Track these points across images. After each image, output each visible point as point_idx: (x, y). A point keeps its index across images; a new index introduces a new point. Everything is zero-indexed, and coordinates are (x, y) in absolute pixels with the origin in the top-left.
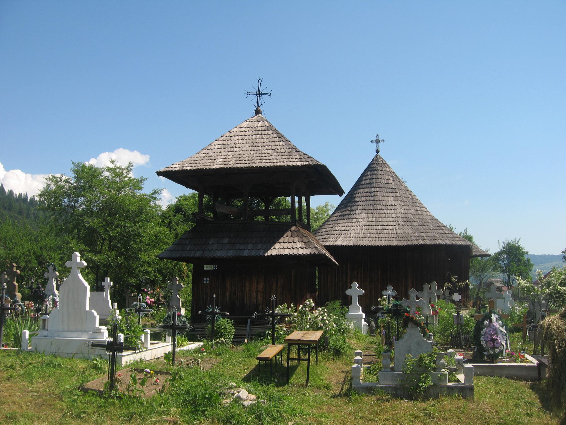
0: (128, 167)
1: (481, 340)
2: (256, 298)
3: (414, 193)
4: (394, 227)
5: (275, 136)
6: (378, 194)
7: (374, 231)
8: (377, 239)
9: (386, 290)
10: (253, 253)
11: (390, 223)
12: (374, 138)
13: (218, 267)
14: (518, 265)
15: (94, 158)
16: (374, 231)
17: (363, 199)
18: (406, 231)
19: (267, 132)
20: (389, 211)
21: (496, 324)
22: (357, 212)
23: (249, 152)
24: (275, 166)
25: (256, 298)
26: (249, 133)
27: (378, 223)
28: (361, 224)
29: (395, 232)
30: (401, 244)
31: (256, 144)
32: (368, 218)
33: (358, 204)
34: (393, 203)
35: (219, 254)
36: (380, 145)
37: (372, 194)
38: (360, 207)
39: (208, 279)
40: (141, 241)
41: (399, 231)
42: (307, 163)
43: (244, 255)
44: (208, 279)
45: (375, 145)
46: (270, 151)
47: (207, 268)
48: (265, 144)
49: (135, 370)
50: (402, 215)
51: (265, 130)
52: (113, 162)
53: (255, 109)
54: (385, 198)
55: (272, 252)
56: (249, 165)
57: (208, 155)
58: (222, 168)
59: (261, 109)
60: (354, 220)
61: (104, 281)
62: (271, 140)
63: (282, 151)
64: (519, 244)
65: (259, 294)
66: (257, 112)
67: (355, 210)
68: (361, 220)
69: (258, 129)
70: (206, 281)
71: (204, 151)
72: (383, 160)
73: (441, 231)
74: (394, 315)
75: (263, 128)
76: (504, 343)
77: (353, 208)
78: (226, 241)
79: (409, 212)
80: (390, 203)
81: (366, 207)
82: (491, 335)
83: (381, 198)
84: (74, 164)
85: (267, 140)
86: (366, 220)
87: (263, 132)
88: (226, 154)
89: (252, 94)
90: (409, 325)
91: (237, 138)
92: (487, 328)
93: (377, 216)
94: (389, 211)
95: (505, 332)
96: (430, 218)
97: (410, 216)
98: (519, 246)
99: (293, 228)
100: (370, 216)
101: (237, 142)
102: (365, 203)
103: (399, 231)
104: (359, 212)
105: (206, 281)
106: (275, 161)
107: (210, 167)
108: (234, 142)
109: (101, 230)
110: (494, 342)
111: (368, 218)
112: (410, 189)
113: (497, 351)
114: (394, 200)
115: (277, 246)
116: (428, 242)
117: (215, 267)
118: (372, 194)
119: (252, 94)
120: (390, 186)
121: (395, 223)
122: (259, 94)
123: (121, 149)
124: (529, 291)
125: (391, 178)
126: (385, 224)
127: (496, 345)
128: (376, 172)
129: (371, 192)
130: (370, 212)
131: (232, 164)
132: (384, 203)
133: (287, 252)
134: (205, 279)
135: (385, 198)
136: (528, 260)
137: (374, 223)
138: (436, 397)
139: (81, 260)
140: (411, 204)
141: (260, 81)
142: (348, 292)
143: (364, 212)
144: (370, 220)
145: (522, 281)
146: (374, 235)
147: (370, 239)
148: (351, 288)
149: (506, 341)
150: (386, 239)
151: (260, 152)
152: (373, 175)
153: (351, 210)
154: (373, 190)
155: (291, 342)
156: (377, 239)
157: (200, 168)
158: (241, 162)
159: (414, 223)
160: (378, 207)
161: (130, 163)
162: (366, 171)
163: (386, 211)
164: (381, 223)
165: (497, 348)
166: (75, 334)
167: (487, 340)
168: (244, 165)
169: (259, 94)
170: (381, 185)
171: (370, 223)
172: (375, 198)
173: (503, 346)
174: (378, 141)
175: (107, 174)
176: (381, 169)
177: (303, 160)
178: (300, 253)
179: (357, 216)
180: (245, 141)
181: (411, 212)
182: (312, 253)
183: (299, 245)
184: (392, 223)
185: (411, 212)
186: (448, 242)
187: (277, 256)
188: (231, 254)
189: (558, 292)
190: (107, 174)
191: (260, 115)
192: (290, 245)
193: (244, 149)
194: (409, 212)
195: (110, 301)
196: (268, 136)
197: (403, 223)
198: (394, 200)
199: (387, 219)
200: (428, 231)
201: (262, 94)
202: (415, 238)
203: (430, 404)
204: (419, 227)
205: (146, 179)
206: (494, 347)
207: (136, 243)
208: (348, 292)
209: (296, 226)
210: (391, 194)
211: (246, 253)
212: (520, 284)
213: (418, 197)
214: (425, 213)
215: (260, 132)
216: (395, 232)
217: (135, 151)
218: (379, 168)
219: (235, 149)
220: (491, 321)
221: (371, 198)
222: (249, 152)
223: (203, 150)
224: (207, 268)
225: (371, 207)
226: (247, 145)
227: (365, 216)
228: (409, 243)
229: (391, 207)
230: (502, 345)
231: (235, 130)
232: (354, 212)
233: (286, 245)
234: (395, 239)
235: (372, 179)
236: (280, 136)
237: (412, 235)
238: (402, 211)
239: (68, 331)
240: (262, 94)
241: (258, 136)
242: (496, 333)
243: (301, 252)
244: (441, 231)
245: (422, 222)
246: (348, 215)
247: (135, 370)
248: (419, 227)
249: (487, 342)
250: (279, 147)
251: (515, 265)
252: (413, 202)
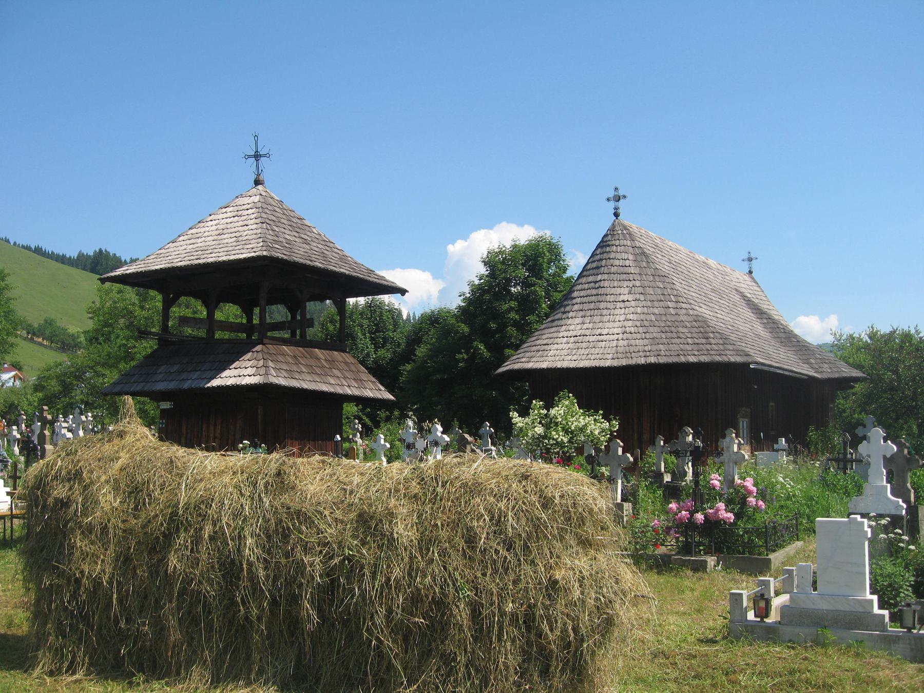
4: (616, 337)
6: (606, 284)
10: (195, 384)
12: (746, 256)
15: (462, 239)
16: (584, 345)
17: (582, 293)
22: (571, 314)
29: (615, 345)
33: (574, 301)
36: (622, 203)
37: (597, 285)
38: (576, 307)
45: (746, 263)
53: (253, 177)
54: (613, 291)
59: (261, 178)
66: (257, 182)
80: (622, 298)
81: (586, 306)
83: (609, 291)
99: (259, 348)
102: (585, 299)
114: (630, 293)
115: (226, 373)
118: (597, 285)
120: (626, 270)
123: (504, 224)
125: (631, 257)
128: (608, 249)
129: (596, 282)
130: (589, 313)
132: (612, 298)
135: (613, 291)
137: (587, 332)
139: (623, 452)
144: (585, 326)
152: (603, 253)
153: (564, 313)
154: (599, 277)
160: (602, 305)
162: (598, 247)
163: (612, 312)
170: (613, 269)
172: (600, 291)
174: (617, 199)
176: (617, 243)
179: (570, 321)
184: (616, 331)
197: (632, 330)
198: (630, 293)
209: (264, 344)
210: (626, 284)
217: (526, 226)
218: (613, 242)
221: (594, 292)
225: (592, 306)
229: (622, 305)
235: (601, 260)
246: (558, 319)
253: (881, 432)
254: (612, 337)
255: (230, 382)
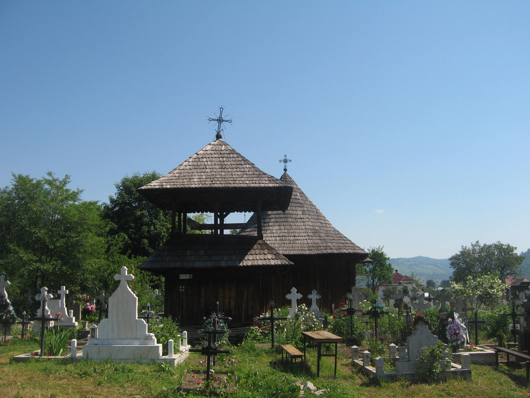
0: (65, 179)
1: (446, 335)
2: (229, 304)
3: (318, 207)
5: (240, 159)
7: (287, 242)
8: (291, 249)
9: (311, 294)
10: (230, 264)
11: (300, 234)
12: (283, 158)
13: (193, 276)
14: (381, 270)
16: (287, 242)
18: (316, 241)
19: (231, 156)
20: (298, 224)
21: (458, 321)
22: (270, 224)
23: (220, 173)
24: (249, 187)
25: (229, 304)
26: (216, 156)
27: (290, 234)
28: (275, 235)
29: (306, 242)
30: (313, 253)
31: (224, 166)
32: (280, 229)
33: (271, 217)
34: (302, 216)
35: (198, 264)
36: (288, 164)
38: (273, 220)
39: (181, 287)
40: (85, 251)
41: (309, 241)
42: (278, 185)
43: (222, 265)
44: (184, 287)
45: (283, 164)
46: (239, 173)
47: (183, 277)
48: (233, 166)
49: (193, 371)
50: (311, 227)
51: (229, 154)
52: (50, 174)
53: (216, 133)
54: (294, 212)
55: (244, 263)
56: (226, 185)
57: (182, 175)
58: (196, 188)
59: (221, 133)
60: (268, 232)
61: (60, 289)
62: (238, 163)
63: (250, 173)
64: (382, 251)
65: (232, 299)
66: (218, 137)
67: (268, 223)
68: (274, 231)
69: (222, 152)
70: (182, 289)
71: (177, 171)
72: (290, 178)
73: (343, 242)
74: (373, 316)
75: (228, 152)
76: (464, 336)
77: (267, 220)
78: (202, 253)
79: (316, 224)
80: (299, 216)
81: (278, 220)
82: (455, 330)
84: (14, 175)
85: (234, 163)
86: (279, 231)
87: (229, 156)
88: (199, 174)
89: (213, 120)
90: (419, 323)
91: (205, 160)
92: (451, 324)
93: (289, 227)
94: (298, 224)
95: (465, 327)
96: (332, 229)
97: (317, 228)
98: (382, 253)
100: (283, 228)
101: (206, 163)
102: (277, 216)
103: (309, 241)
104: (272, 224)
105: (182, 289)
106: (247, 182)
107: (189, 186)
108: (203, 163)
109: (47, 240)
110: (457, 336)
111: (280, 229)
112: (314, 204)
113: (459, 342)
115: (249, 257)
116: (335, 251)
117: (190, 276)
119: (213, 120)
121: (305, 234)
122: (220, 120)
124: (463, 293)
125: (298, 194)
126: (297, 235)
127: (459, 338)
130: (282, 224)
131: (208, 184)
133: (260, 263)
134: (181, 287)
135: (294, 212)
136: (390, 265)
137: (285, 234)
138: (445, 380)
140: (317, 217)
141: (222, 109)
142: (288, 297)
143: (277, 224)
145: (455, 285)
146: (288, 245)
147: (285, 249)
148: (290, 293)
149: (466, 334)
150: (299, 248)
151: (231, 173)
155: (319, 341)
156: (291, 249)
157: (179, 186)
158: (217, 182)
159: (322, 235)
160: (289, 220)
161: (66, 176)
164: (293, 234)
165: (459, 340)
166: (126, 341)
167: (452, 334)
168: (221, 186)
169: (220, 120)
171: (283, 234)
173: (464, 338)
174: (285, 161)
175: (47, 186)
177: (273, 182)
178: (273, 264)
180: (213, 163)
181: (318, 224)
182: (283, 263)
183: (270, 256)
184: (303, 234)
185: (318, 224)
186: (351, 251)
187: (252, 267)
188: (209, 264)
189: (489, 294)
190: (47, 186)
191: (221, 139)
192: (262, 257)
193: (214, 170)
194: (316, 224)
195: (66, 308)
196: (234, 159)
197: (312, 234)
199: (298, 231)
200: (333, 241)
201: (223, 121)
202: (323, 248)
203: (442, 386)
204: (325, 238)
205: (82, 191)
206: (457, 340)
207: (79, 252)
208: (288, 297)
210: (299, 209)
211: (223, 264)
212: (454, 287)
213: (321, 211)
214: (328, 226)
215: (225, 155)
216: (306, 242)
219: (207, 170)
220: (453, 318)
222: (220, 173)
223: (175, 169)
224: (183, 277)
225: (283, 220)
226: (217, 167)
227: (277, 228)
228: (320, 252)
229: (301, 220)
230: (463, 337)
231: (201, 152)
232: (267, 224)
233: (258, 257)
234: (306, 249)
236: (245, 160)
237: (321, 245)
238: (310, 223)
239: (119, 339)
240: (223, 121)
241: (225, 159)
242: (458, 328)
243: (273, 262)
244: (343, 242)
245: (327, 234)
247: (193, 371)
248: (325, 238)
249: (451, 336)
250: (246, 170)
251: (379, 269)
252: (318, 216)
253: (318, 298)
254: (302, 238)
255: (250, 263)
